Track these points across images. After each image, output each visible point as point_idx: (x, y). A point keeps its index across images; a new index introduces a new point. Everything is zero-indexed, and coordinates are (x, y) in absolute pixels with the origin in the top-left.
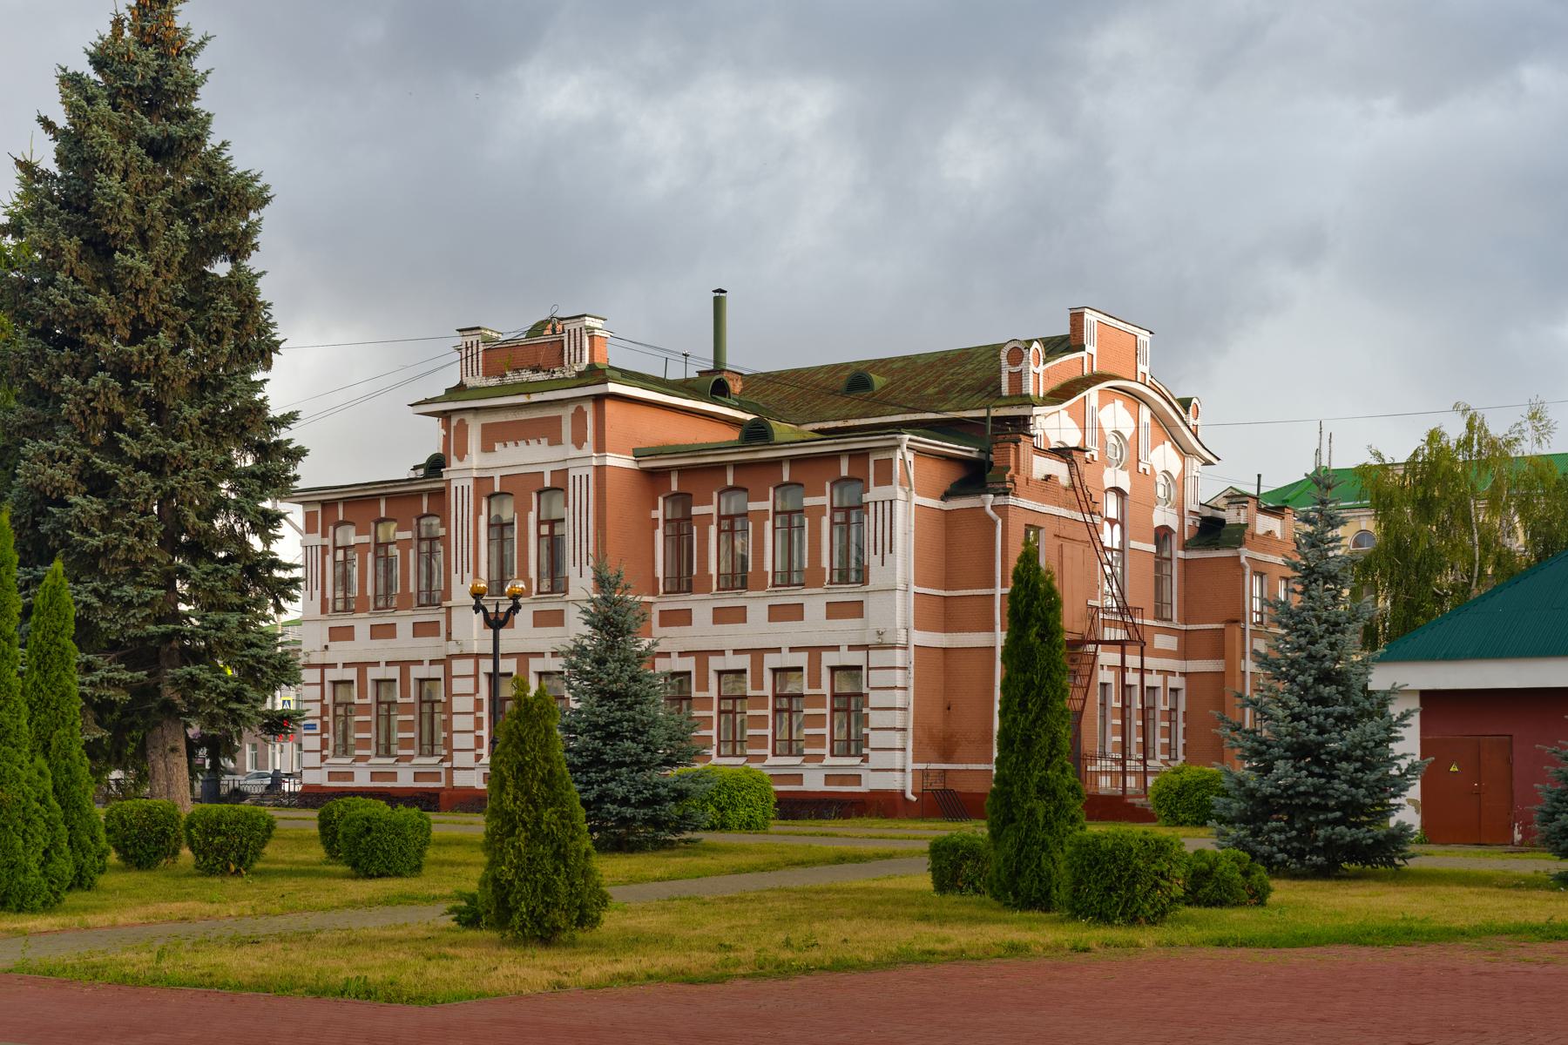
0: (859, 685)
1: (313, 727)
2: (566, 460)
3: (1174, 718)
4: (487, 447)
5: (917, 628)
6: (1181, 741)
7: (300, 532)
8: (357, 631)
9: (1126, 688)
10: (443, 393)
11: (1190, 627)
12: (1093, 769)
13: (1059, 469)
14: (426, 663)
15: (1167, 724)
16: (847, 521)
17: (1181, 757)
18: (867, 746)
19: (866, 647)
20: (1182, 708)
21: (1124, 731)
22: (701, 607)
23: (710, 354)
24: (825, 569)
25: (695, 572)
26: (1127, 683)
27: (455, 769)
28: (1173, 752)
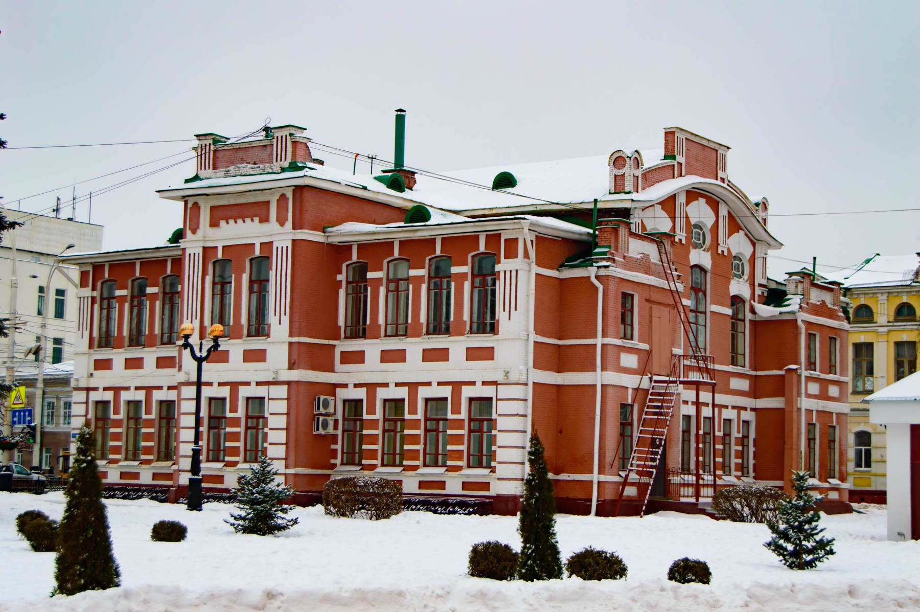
0: (491, 414)
2: (271, 235)
4: (214, 224)
5: (535, 367)
6: (752, 462)
7: (76, 286)
8: (145, 361)
11: (759, 373)
13: (651, 250)
14: (165, 388)
15: (740, 448)
16: (397, 290)
18: (495, 460)
19: (495, 383)
20: (752, 435)
22: (372, 348)
23: (392, 158)
24: (340, 327)
25: (368, 322)
28: (745, 470)
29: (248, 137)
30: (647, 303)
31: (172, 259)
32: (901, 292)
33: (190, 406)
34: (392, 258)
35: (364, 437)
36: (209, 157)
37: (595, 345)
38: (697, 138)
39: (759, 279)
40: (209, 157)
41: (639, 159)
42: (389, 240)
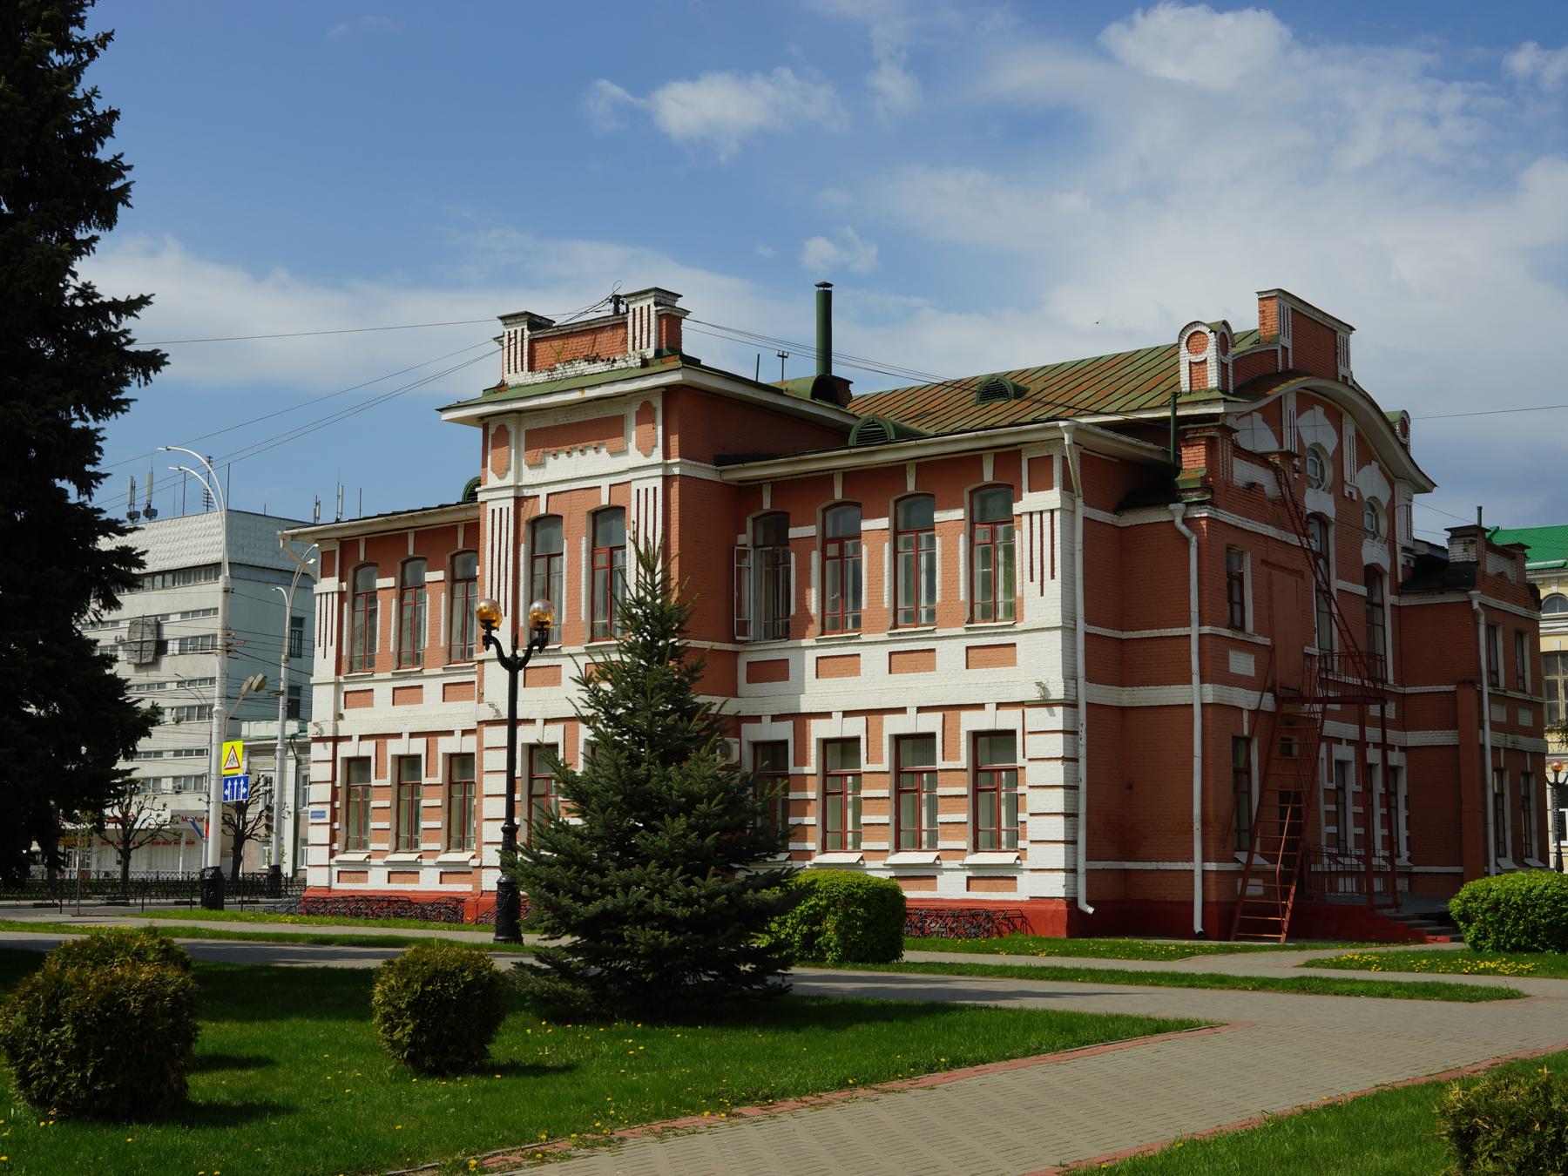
1: (321, 814)
3: (1341, 800)
9: (1366, 770)
10: (480, 394)
12: (1319, 868)
14: (458, 734)
17: (1405, 853)
20: (1403, 790)
21: (1365, 820)
25: (793, 611)
26: (1390, 763)
27: (484, 867)
29: (586, 312)
30: (1264, 567)
31: (466, 525)
32: (1549, 578)
33: (499, 760)
34: (830, 502)
35: (791, 804)
36: (522, 350)
37: (1189, 636)
38: (1308, 309)
39: (1401, 540)
40: (522, 350)
41: (1228, 336)
42: (826, 473)
